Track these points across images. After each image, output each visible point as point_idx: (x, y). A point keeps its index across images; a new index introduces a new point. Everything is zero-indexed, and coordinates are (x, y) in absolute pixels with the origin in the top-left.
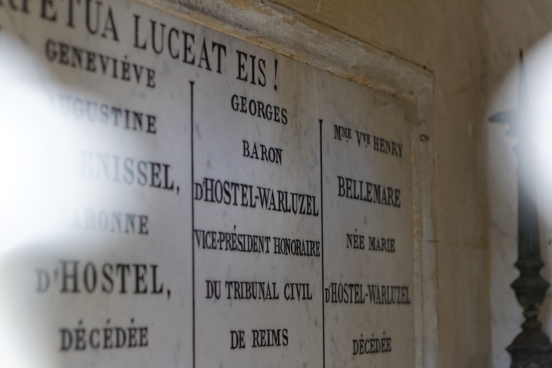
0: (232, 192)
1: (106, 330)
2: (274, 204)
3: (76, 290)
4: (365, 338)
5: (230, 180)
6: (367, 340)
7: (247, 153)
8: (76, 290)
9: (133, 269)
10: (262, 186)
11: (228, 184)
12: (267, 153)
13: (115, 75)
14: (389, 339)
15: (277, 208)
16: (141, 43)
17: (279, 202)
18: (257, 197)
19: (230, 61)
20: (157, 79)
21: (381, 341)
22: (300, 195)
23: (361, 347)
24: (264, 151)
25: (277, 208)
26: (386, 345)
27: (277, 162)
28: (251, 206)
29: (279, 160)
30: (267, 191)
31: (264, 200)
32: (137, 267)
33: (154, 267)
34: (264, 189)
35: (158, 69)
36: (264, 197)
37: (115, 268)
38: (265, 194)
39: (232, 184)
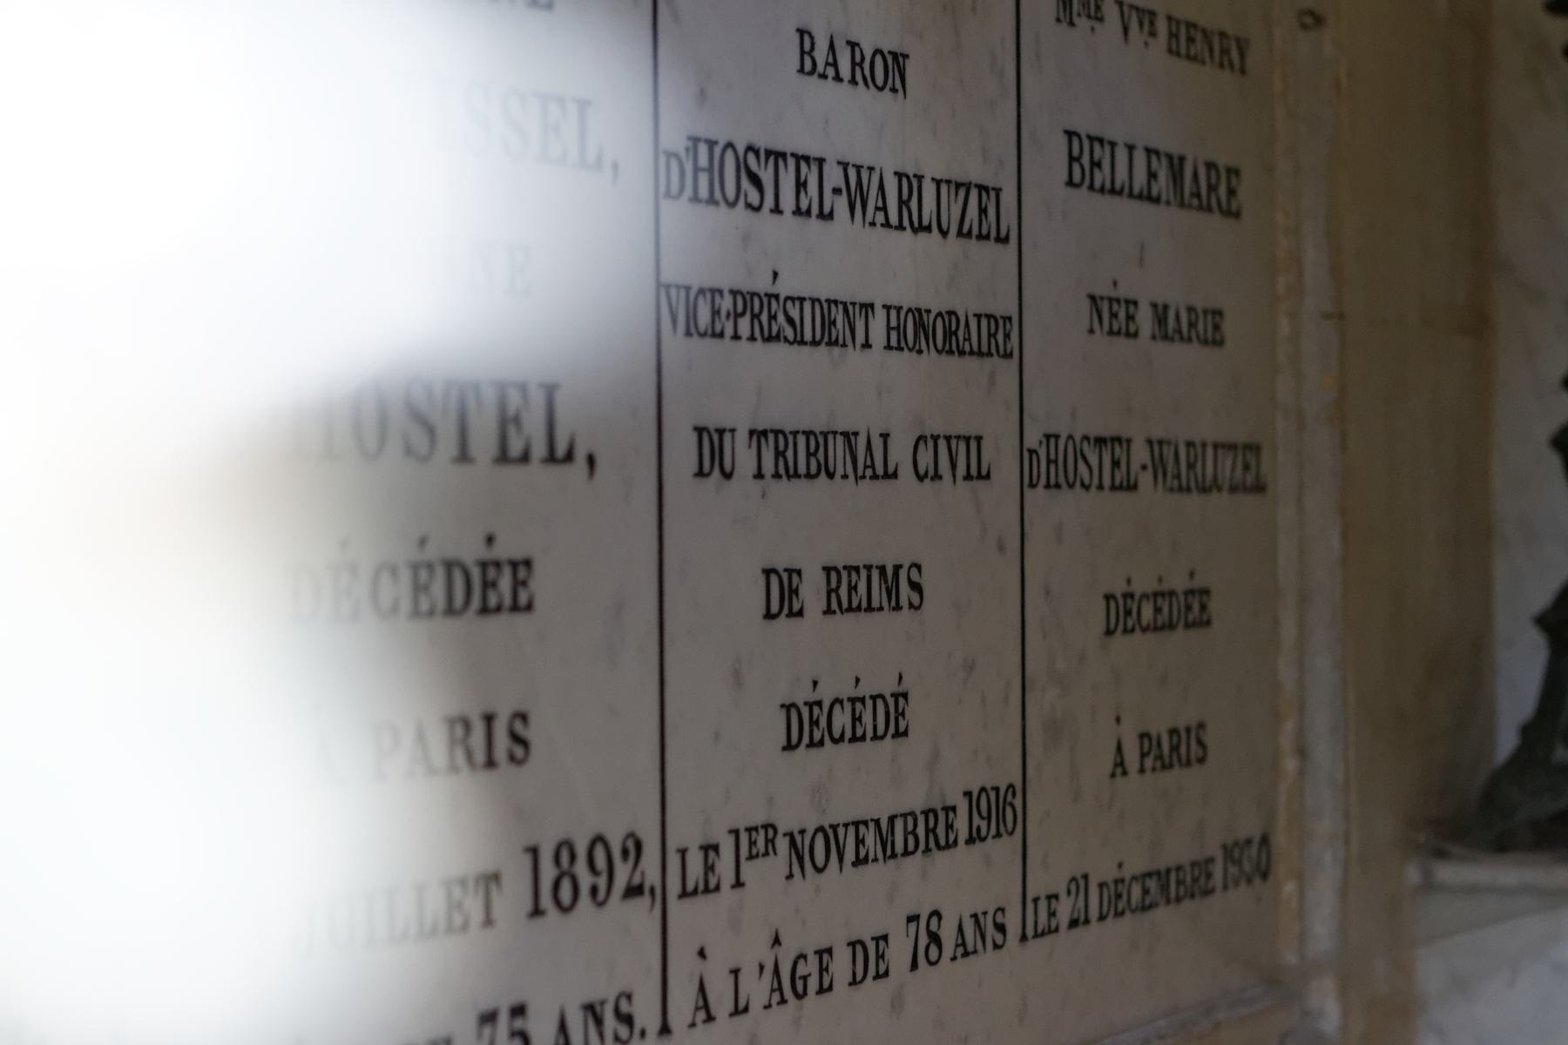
0: (766, 177)
1: (853, 700)
2: (884, 209)
4: (826, 694)
5: (762, 143)
6: (1145, 596)
7: (808, 66)
11: (757, 153)
12: (867, 65)
14: (1205, 592)
15: (894, 220)
22: (958, 185)
23: (814, 723)
24: (858, 59)
25: (894, 220)
27: (894, 90)
29: (898, 85)
31: (857, 198)
34: (858, 168)
39: (769, 153)
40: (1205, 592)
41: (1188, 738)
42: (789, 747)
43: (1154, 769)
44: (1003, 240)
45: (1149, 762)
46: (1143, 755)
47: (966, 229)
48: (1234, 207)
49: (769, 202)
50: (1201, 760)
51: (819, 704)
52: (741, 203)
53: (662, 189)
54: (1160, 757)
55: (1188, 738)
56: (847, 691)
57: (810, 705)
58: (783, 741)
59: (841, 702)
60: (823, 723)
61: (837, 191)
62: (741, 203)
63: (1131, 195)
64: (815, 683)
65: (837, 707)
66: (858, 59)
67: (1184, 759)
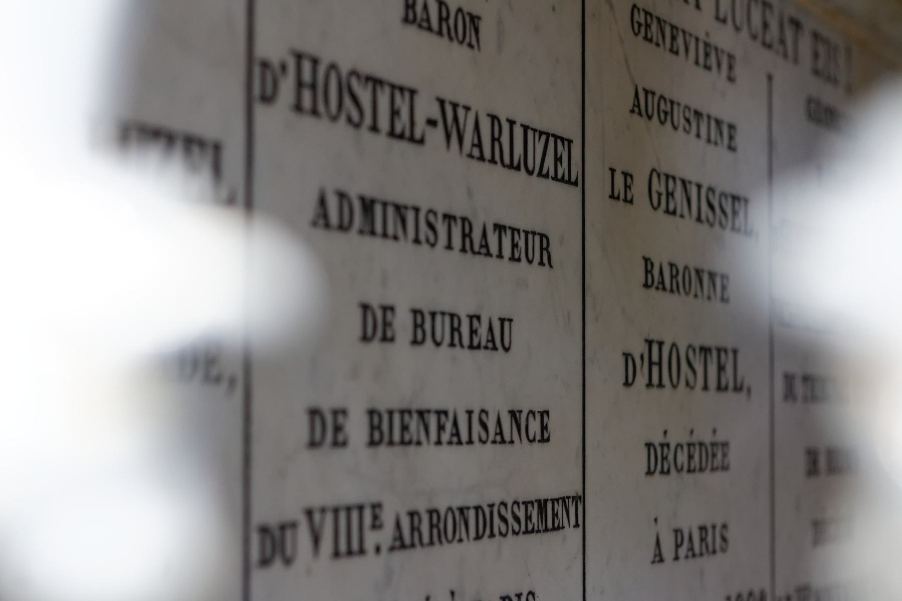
0: (365, 96)
1: (689, 445)
3: (661, 385)
4: (673, 440)
5: (366, 68)
6: (679, 445)
7: (411, 16)
8: (661, 385)
9: (714, 353)
10: (448, 97)
12: (451, 21)
13: (697, 63)
14: (725, 445)
15: (487, 154)
16: (721, 16)
17: (497, 144)
18: (432, 123)
19: (806, 45)
20: (738, 71)
21: (379, 314)
22: (541, 133)
23: (664, 458)
24: (444, 15)
25: (487, 154)
26: (719, 456)
27: (470, 46)
28: (625, 200)
29: (474, 42)
30: (461, 112)
31: (453, 131)
32: (719, 350)
33: (735, 352)
34: (455, 106)
35: (738, 54)
36: (450, 119)
37: (697, 351)
38: (456, 118)
40: (725, 445)
41: (714, 533)
42: (649, 473)
43: (687, 557)
44: (575, 184)
45: (683, 552)
46: (678, 546)
47: (544, 172)
48: (447, 220)
49: (368, 120)
50: (723, 550)
51: (668, 445)
52: (343, 118)
53: (257, 90)
54: (691, 549)
55: (714, 533)
56: (685, 439)
57: (662, 445)
58: (645, 469)
59: (682, 447)
60: (671, 457)
61: (432, 123)
62: (343, 118)
63: (555, 178)
64: (665, 432)
65: (679, 450)
66: (444, 15)
67: (711, 548)
